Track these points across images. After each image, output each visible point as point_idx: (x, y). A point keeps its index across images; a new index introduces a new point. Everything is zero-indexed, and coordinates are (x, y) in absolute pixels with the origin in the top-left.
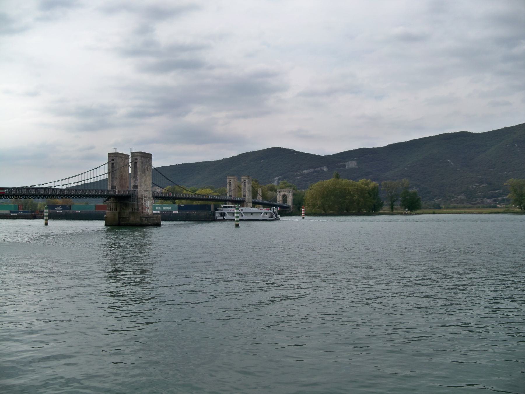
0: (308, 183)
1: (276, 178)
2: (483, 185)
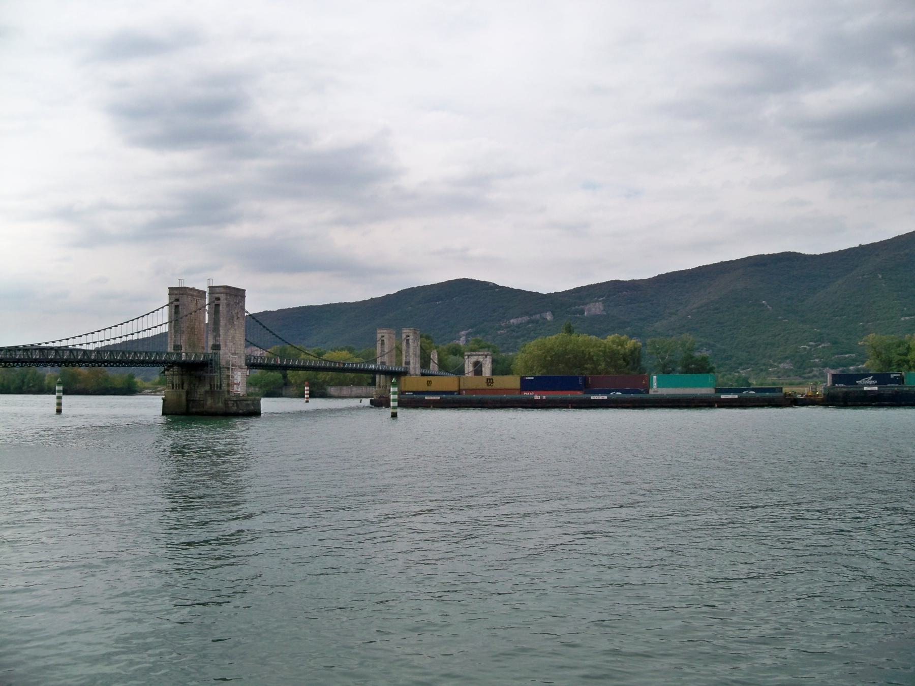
0: (518, 340)
1: (463, 333)
2: (823, 345)
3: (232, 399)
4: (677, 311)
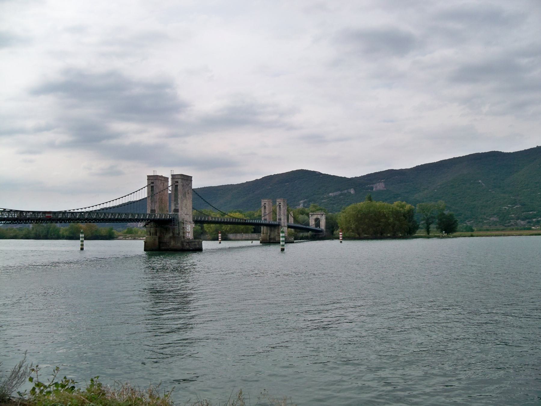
0: (334, 206)
1: (302, 201)
2: (516, 206)
3: (186, 241)
4: (428, 187)
